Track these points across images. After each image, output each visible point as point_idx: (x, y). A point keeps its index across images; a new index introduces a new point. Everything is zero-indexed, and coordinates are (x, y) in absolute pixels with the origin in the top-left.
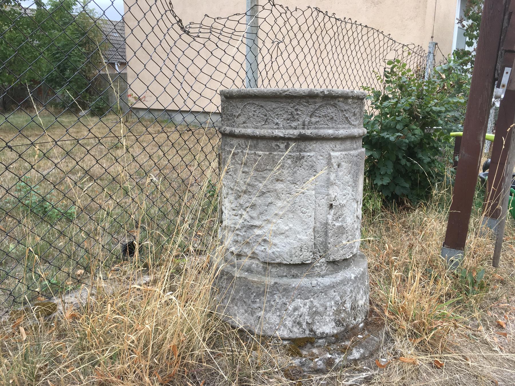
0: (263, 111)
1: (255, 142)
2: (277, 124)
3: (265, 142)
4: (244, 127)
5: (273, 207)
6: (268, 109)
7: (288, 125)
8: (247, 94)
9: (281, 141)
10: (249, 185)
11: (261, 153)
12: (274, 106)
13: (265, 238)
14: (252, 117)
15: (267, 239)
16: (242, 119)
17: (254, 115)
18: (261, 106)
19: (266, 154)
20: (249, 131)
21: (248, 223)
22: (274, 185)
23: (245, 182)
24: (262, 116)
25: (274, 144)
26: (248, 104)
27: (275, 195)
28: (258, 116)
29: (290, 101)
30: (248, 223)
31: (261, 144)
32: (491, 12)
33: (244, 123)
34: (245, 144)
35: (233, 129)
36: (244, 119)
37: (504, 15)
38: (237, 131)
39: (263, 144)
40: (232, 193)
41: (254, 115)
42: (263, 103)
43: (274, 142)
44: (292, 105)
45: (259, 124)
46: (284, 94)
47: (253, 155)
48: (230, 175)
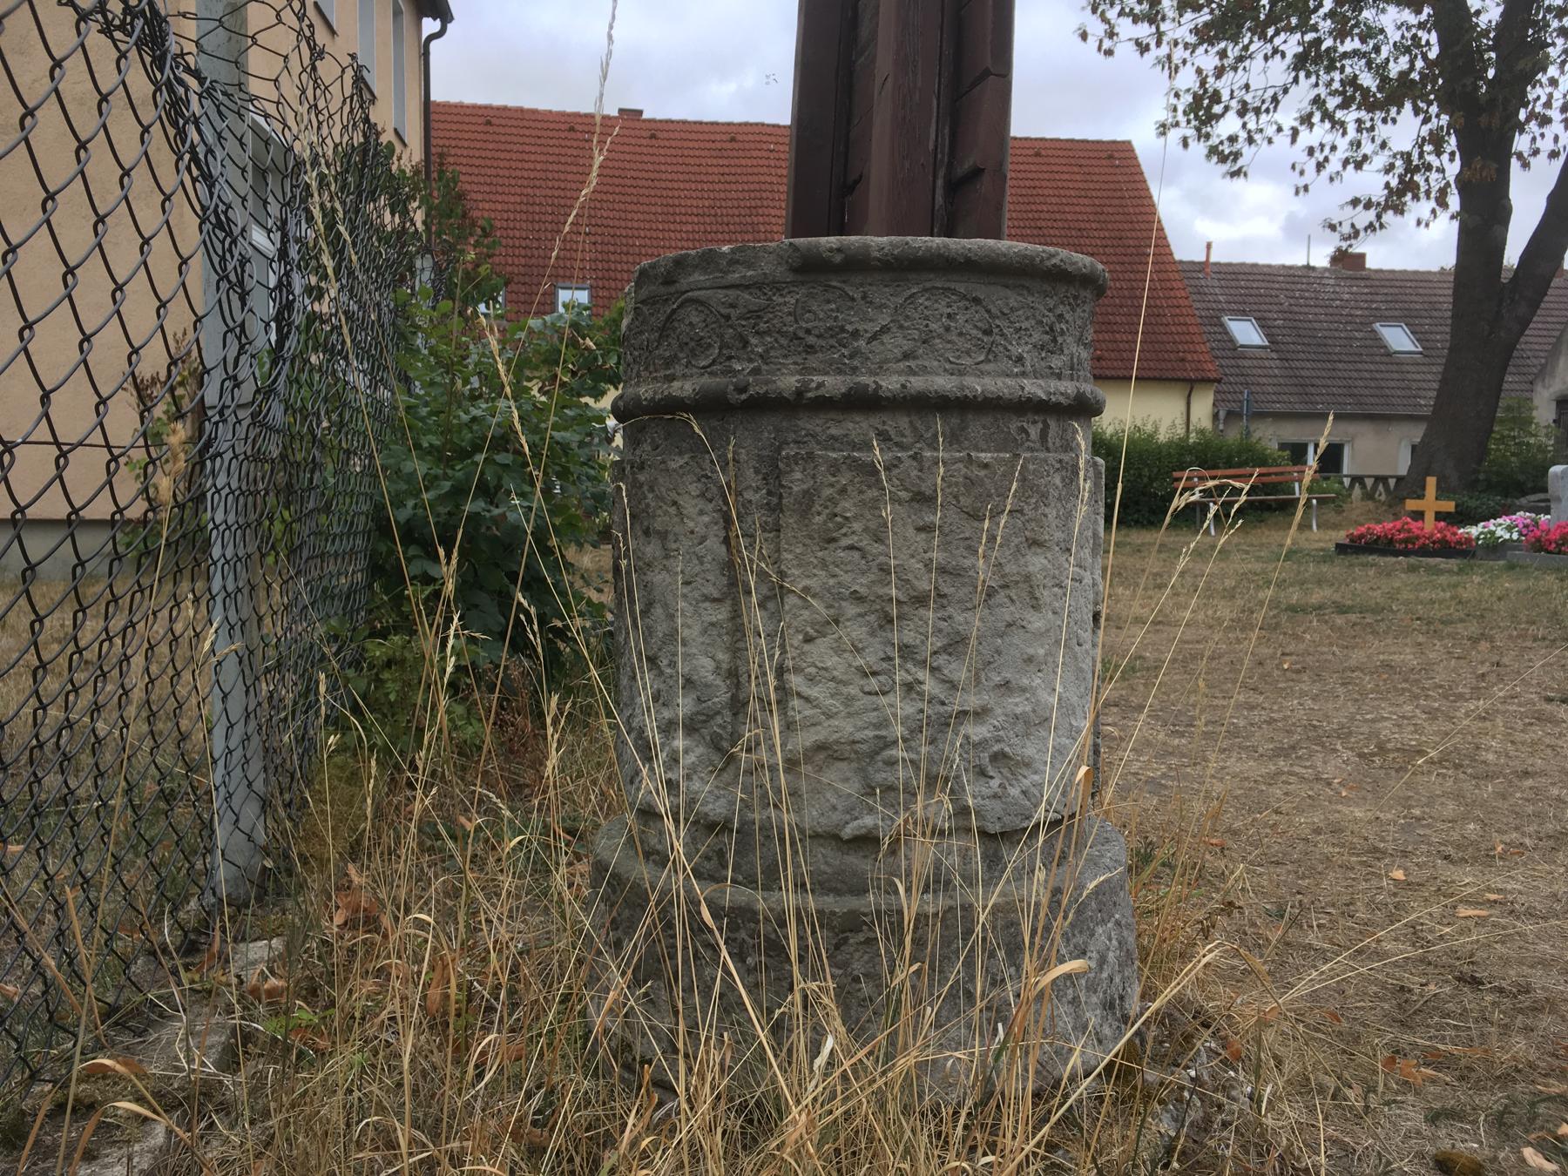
0: (978, 314)
1: (955, 421)
2: (1020, 359)
3: (987, 420)
4: (911, 372)
5: (1017, 638)
6: (994, 310)
7: (1043, 364)
8: (940, 256)
9: (1030, 416)
10: (942, 570)
11: (986, 457)
12: (1013, 303)
13: (996, 748)
14: (940, 336)
15: (1007, 749)
16: (894, 343)
17: (948, 329)
18: (976, 301)
19: (1003, 459)
20: (943, 383)
21: (942, 709)
22: (1022, 561)
23: (927, 565)
24: (974, 332)
25: (1014, 425)
26: (926, 290)
27: (1024, 594)
28: (961, 334)
29: (1047, 287)
30: (942, 709)
31: (977, 427)
32: (907, 165)
33: (906, 356)
34: (915, 429)
35: (865, 379)
36: (907, 346)
37: (935, 177)
38: (891, 383)
39: (984, 427)
40: (861, 615)
41: (948, 329)
42: (980, 291)
43: (1015, 418)
44: (1051, 303)
45: (967, 361)
46: (1048, 263)
47: (960, 465)
48: (851, 548)
